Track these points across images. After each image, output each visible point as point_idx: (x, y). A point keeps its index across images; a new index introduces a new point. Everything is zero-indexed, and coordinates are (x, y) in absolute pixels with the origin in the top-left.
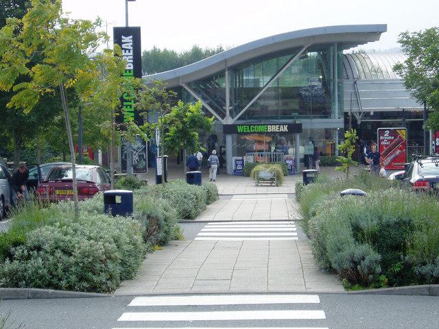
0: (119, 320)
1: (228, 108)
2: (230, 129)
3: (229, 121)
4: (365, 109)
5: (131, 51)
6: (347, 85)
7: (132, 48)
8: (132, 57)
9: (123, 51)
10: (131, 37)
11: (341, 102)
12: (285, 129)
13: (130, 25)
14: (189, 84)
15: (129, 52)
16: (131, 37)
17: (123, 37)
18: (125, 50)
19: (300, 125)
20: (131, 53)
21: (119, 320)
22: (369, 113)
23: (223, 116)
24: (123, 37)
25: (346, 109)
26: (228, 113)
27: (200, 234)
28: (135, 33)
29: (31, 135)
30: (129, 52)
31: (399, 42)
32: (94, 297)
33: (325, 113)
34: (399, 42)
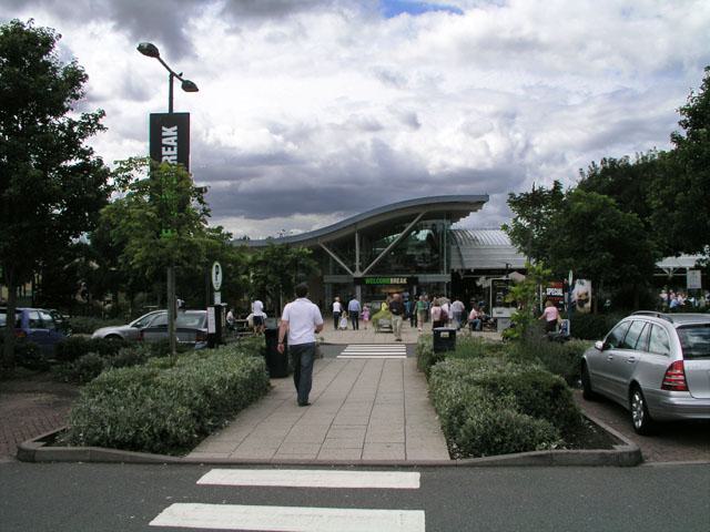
0: (152, 523)
1: (358, 264)
2: (359, 281)
3: (358, 274)
4: (467, 267)
5: (175, 149)
6: (454, 247)
7: (175, 144)
8: (175, 158)
9: (164, 149)
10: (176, 128)
11: (448, 261)
12: (405, 281)
13: (175, 110)
14: (328, 245)
15: (172, 150)
16: (176, 128)
17: (164, 128)
18: (167, 146)
19: (417, 278)
20: (175, 152)
21: (152, 523)
22: (469, 270)
23: (353, 270)
24: (164, 128)
25: (452, 267)
26: (357, 267)
27: (213, 477)
28: (181, 122)
29: (649, 305)
30: (172, 150)
31: (556, 183)
32: (161, 463)
33: (435, 269)
34: (556, 183)
